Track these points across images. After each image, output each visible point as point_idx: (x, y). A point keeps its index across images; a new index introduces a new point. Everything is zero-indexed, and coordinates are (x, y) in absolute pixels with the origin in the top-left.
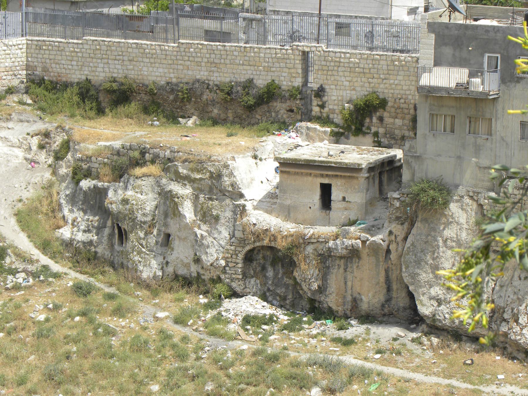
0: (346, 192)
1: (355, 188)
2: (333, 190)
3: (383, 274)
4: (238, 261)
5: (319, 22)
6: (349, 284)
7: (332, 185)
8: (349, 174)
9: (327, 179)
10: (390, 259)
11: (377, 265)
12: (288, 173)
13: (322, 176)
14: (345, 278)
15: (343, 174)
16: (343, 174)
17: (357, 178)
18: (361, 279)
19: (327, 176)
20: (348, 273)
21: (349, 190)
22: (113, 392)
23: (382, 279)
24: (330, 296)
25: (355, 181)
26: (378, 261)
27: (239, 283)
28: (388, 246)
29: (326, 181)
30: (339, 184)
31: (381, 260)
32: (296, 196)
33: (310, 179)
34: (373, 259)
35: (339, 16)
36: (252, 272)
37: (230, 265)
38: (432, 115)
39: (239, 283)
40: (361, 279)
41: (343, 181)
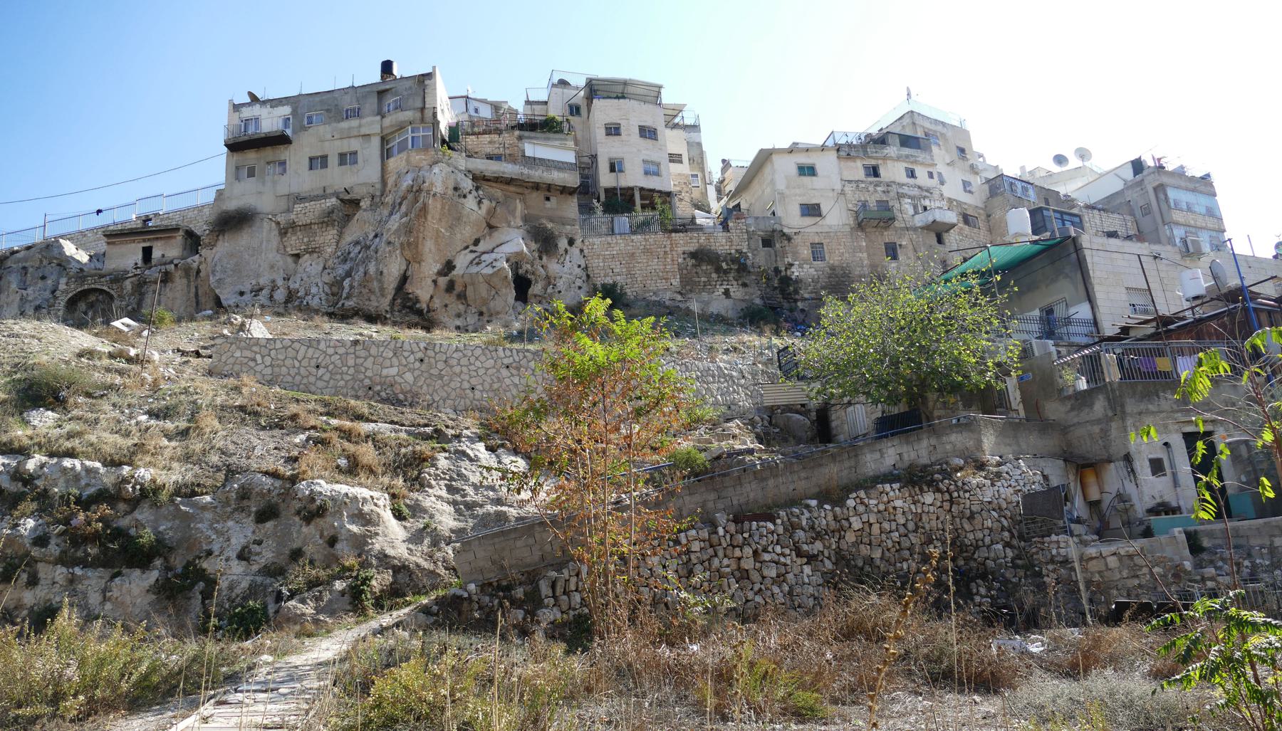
3: (193, 290)
11: (189, 286)
12: (113, 243)
13: (144, 241)
23: (192, 295)
26: (189, 281)
34: (185, 281)
38: (237, 168)
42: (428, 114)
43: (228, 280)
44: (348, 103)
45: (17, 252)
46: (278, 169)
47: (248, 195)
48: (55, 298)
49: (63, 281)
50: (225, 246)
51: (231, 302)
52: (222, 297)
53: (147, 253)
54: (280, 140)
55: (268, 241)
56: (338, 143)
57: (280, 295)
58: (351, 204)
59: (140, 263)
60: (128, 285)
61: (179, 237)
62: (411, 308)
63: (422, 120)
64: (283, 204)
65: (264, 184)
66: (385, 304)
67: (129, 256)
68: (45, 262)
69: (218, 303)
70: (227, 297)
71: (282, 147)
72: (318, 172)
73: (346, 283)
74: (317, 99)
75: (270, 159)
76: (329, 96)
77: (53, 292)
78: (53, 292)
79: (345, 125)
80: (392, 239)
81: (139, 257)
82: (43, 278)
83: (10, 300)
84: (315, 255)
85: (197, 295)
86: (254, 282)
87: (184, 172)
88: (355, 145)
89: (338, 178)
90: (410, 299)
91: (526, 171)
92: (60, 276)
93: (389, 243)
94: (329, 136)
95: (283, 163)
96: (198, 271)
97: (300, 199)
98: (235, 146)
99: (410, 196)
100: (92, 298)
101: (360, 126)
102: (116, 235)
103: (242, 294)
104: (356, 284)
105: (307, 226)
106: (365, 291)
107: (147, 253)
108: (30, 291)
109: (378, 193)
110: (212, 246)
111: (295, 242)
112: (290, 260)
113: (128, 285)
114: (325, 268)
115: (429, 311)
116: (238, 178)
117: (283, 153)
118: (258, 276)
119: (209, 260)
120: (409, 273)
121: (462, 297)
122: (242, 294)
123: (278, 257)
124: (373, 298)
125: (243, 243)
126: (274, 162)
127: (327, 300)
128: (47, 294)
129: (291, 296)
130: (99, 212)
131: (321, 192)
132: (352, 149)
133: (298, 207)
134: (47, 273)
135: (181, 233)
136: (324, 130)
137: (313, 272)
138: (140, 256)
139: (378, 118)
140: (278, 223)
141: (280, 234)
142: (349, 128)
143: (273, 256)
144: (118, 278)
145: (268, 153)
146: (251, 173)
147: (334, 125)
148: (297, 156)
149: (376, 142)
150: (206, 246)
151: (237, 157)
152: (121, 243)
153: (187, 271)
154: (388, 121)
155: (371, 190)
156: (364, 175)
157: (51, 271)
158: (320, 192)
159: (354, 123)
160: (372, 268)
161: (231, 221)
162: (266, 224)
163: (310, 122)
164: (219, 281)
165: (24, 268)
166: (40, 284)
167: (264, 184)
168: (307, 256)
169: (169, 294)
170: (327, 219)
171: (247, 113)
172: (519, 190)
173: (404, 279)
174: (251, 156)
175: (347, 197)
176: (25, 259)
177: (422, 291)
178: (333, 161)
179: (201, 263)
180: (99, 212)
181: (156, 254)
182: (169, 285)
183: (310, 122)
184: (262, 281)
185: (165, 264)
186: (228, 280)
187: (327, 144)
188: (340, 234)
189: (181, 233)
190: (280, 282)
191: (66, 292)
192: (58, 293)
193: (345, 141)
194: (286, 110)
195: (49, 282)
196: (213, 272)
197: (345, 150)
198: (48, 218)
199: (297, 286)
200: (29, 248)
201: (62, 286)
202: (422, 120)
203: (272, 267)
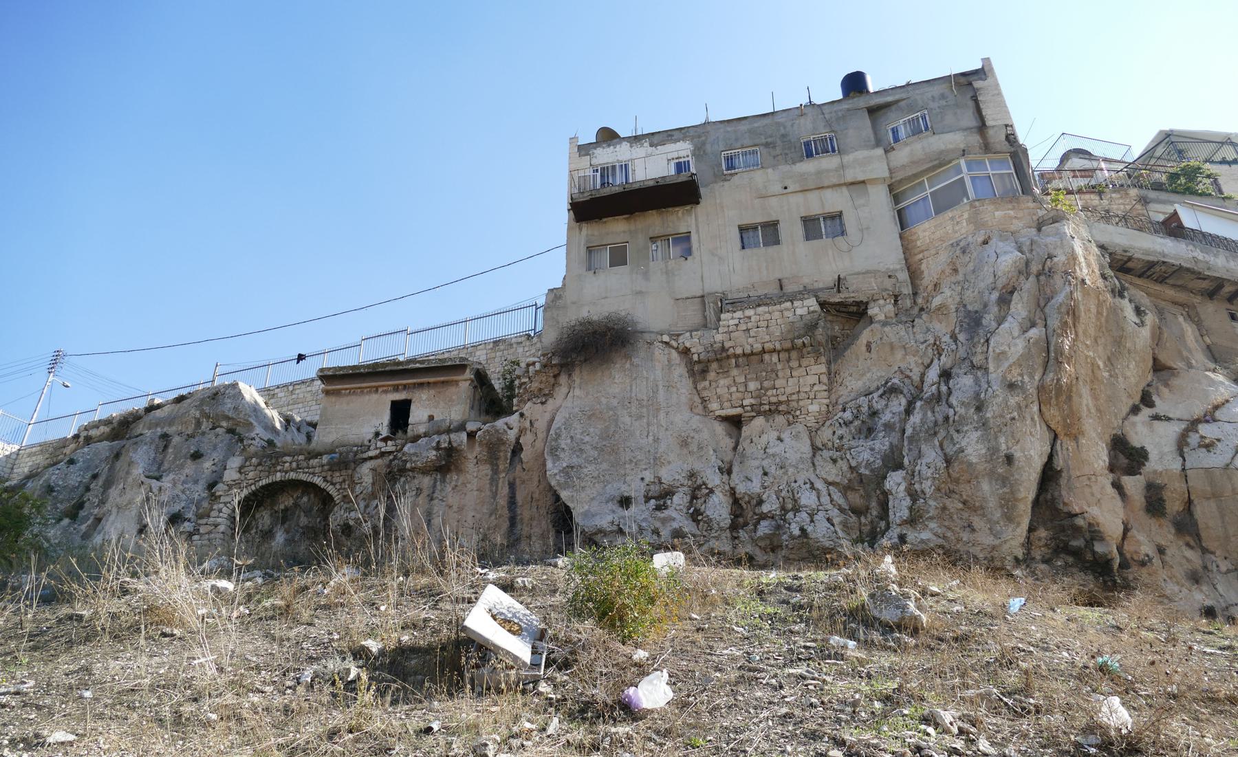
3: (504, 491)
5: (828, 187)
10: (521, 461)
11: (494, 481)
12: (337, 393)
13: (396, 389)
15: (432, 380)
16: (432, 380)
17: (457, 382)
19: (405, 387)
20: (436, 502)
22: (298, 419)
23: (502, 501)
25: (453, 389)
26: (496, 471)
28: (518, 439)
31: (501, 467)
33: (375, 397)
34: (486, 470)
35: (698, 231)
38: (590, 250)
40: (461, 509)
41: (432, 392)
42: (997, 137)
43: (589, 469)
44: (806, 130)
45: (159, 406)
46: (674, 251)
47: (609, 295)
48: (214, 498)
49: (235, 462)
50: (573, 400)
51: (604, 522)
52: (578, 511)
53: (400, 413)
54: (679, 193)
55: (669, 387)
56: (799, 198)
57: (718, 508)
58: (852, 313)
59: (385, 432)
60: (365, 473)
61: (464, 384)
62: (1076, 553)
63: (987, 147)
64: (692, 315)
65: (646, 275)
66: (1014, 538)
67: (367, 418)
68: (205, 425)
69: (562, 519)
70: (590, 509)
71: (680, 211)
72: (761, 253)
73: (895, 482)
74: (743, 127)
75: (657, 230)
76: (784, 115)
77: (211, 486)
78: (211, 486)
79: (808, 166)
80: (1014, 376)
81: (383, 421)
82: (197, 456)
83: (123, 501)
84: (780, 420)
85: (512, 502)
86: (649, 477)
87: (485, 267)
88: (834, 201)
89: (812, 264)
90: (1077, 530)
91: (1200, 256)
92: (230, 453)
93: (1012, 386)
94: (777, 188)
95: (685, 239)
96: (517, 449)
97: (726, 303)
98: (586, 210)
99: (1029, 285)
100: (286, 501)
101: (843, 167)
102: (338, 380)
103: (625, 502)
104: (928, 487)
105: (753, 358)
106: (954, 505)
107: (400, 413)
108: (166, 482)
109: (907, 290)
110: (544, 396)
111: (728, 391)
112: (720, 428)
113: (365, 473)
114: (815, 449)
115: (1124, 565)
116: (591, 267)
117: (681, 220)
118: (657, 461)
119: (541, 425)
120: (1059, 463)
121: (1186, 526)
122: (625, 502)
123: (696, 421)
124: (977, 522)
125: (615, 389)
126: (664, 238)
127: (845, 525)
128: (199, 491)
129: (743, 511)
130: (301, 357)
131: (773, 290)
132: (831, 208)
133: (728, 319)
134: (205, 448)
135: (468, 374)
136: (769, 178)
137: (792, 457)
138: (386, 418)
139: (880, 151)
140: (686, 352)
141: (692, 373)
142: (819, 173)
143: (683, 419)
144: (345, 460)
145: (654, 222)
146: (618, 258)
147: (785, 168)
148: (713, 222)
149: (879, 197)
150: (533, 396)
151: (590, 231)
152: (352, 392)
153: (493, 447)
154: (902, 156)
155: (888, 283)
156: (868, 253)
157: (214, 442)
158: (773, 290)
159: (828, 163)
160: (972, 446)
161: (592, 345)
162: (659, 352)
163: (730, 167)
164: (567, 471)
165: (165, 437)
166: (190, 468)
167: (646, 275)
168: (760, 421)
169: (453, 499)
170: (798, 345)
171: (605, 156)
172: (1182, 296)
173: (1049, 475)
174: (616, 229)
175: (837, 299)
176: (171, 421)
177: (1102, 507)
178: (791, 231)
179: (522, 431)
180: (301, 357)
181: (418, 415)
182: (453, 477)
183: (730, 167)
184: (671, 473)
185: (449, 431)
186: (589, 469)
187: (774, 201)
188: (832, 375)
189: (468, 374)
190: (714, 479)
191: (237, 484)
192: (220, 489)
193: (813, 196)
194: (683, 149)
195: (207, 465)
196: (554, 451)
197: (815, 209)
198: (219, 370)
199: (755, 487)
200: (180, 399)
201: (230, 475)
202: (987, 147)
203: (684, 443)
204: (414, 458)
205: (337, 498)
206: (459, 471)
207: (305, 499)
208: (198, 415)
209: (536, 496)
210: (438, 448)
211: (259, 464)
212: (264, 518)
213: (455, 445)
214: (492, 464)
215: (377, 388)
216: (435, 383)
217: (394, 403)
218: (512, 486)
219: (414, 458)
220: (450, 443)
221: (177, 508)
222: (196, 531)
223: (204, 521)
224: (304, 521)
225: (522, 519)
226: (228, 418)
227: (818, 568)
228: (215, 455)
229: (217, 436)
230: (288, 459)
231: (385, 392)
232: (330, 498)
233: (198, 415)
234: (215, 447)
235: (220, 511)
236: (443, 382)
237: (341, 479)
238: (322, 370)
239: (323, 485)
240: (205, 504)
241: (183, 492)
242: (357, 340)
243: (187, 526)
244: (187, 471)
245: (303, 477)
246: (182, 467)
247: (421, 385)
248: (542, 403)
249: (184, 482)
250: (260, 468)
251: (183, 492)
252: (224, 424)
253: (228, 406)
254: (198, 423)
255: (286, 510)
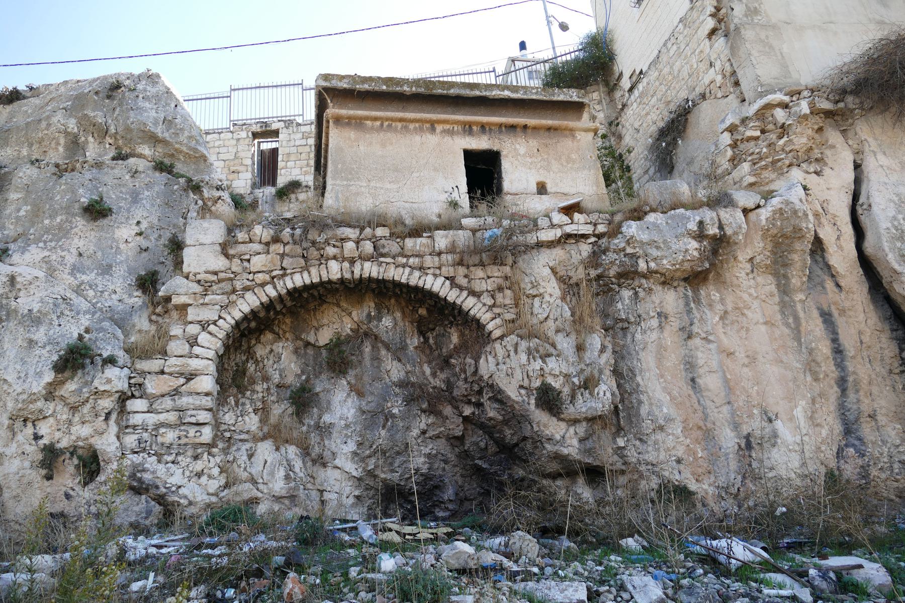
0: (548, 169)
1: (569, 160)
2: (507, 165)
3: (814, 327)
4: (195, 364)
6: (711, 382)
7: (503, 153)
8: (550, 122)
9: (485, 138)
11: (786, 306)
13: (468, 129)
14: (690, 365)
15: (532, 122)
16: (532, 122)
18: (752, 359)
19: (483, 127)
20: (697, 341)
21: (555, 166)
24: (659, 436)
26: (784, 289)
27: (199, 466)
29: (480, 143)
30: (522, 150)
31: (795, 281)
32: (389, 186)
33: (432, 140)
34: (767, 284)
36: (252, 422)
37: (152, 386)
39: (199, 466)
41: (534, 143)
53: (483, 173)
67: (421, 174)
100: (332, 326)
128: (118, 290)
152: (386, 125)
166: (83, 236)
169: (730, 339)
181: (517, 176)
204: (654, 253)
205: (493, 326)
206: (721, 282)
207: (387, 322)
208: (72, 125)
209: (866, 339)
210: (700, 235)
211: (276, 240)
212: (281, 360)
213: (729, 231)
214: (776, 275)
215: (433, 124)
216: (535, 128)
217: (469, 156)
218: (827, 317)
219: (654, 253)
220: (721, 227)
221: (72, 331)
222: (136, 390)
223: (154, 364)
224: (395, 370)
225: (856, 383)
226: (154, 140)
227: (550, 384)
228: (139, 213)
229: (135, 173)
230: (352, 233)
231: (451, 133)
232: (478, 325)
233: (72, 125)
234: (135, 198)
235: (193, 342)
236: (549, 129)
237: (490, 285)
238: (326, 77)
239: (452, 296)
240: (142, 322)
241: (78, 290)
242: (225, 90)
243: (115, 378)
244: (78, 243)
245: (402, 275)
246: (63, 232)
247: (512, 127)
248: (817, 173)
249: (75, 270)
250: (279, 248)
251: (78, 290)
252: (146, 150)
253: (150, 115)
254: (75, 145)
255: (336, 345)
